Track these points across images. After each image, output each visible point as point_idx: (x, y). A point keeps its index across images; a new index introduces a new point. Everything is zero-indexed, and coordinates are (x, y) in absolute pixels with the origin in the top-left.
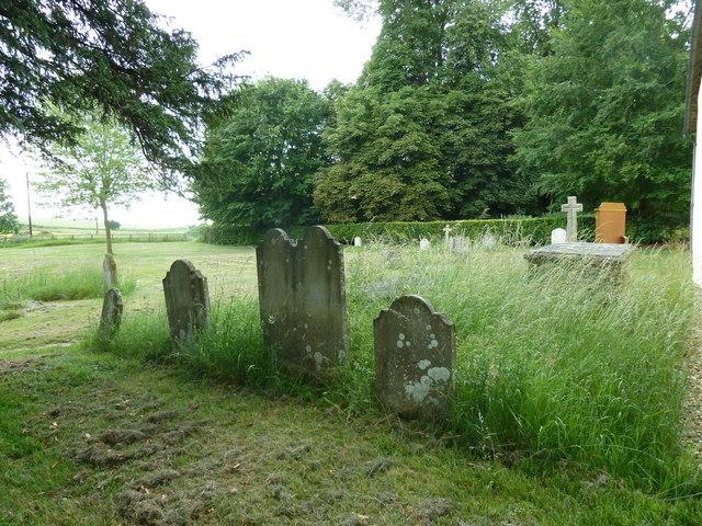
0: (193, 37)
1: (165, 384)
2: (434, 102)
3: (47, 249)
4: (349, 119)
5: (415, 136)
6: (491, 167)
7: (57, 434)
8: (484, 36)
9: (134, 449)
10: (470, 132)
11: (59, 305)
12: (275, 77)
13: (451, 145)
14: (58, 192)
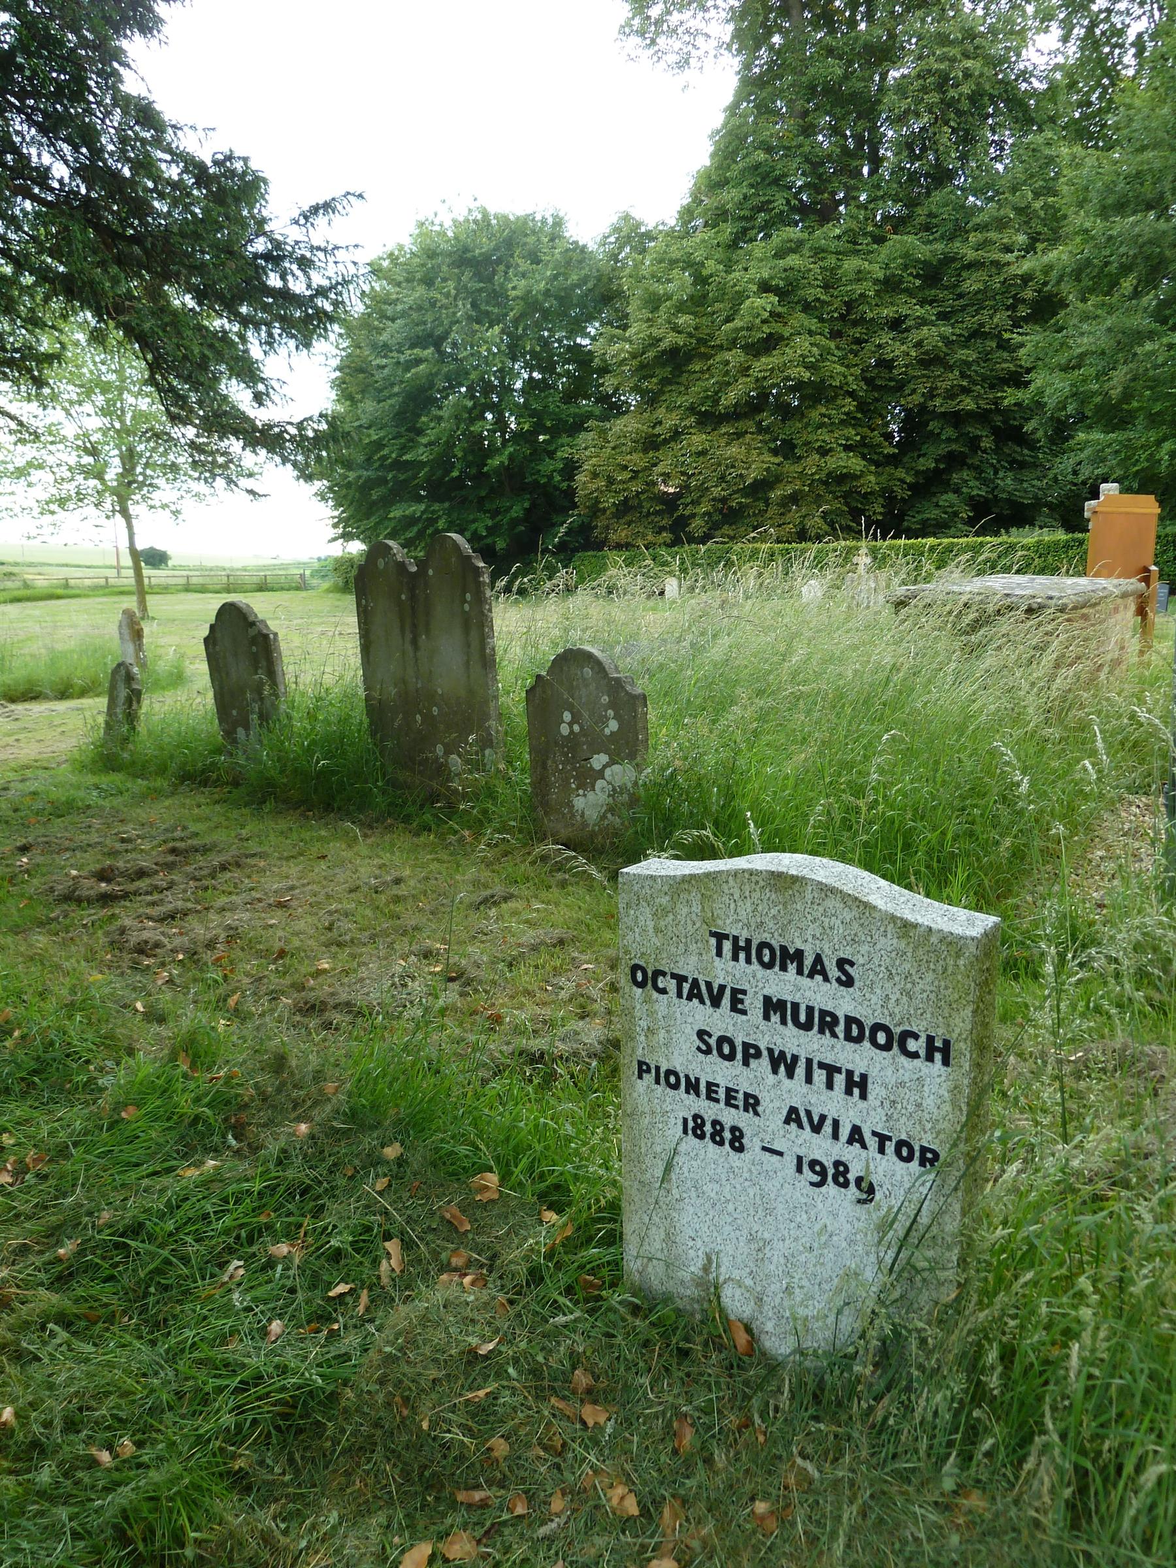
0: (253, 165)
1: (206, 810)
2: (851, 264)
3: (13, 610)
4: (656, 309)
5: (802, 344)
6: (982, 417)
7: (27, 871)
8: (975, 98)
9: (143, 884)
10: (931, 335)
11: (37, 708)
12: (492, 210)
13: (886, 364)
14: (30, 485)
